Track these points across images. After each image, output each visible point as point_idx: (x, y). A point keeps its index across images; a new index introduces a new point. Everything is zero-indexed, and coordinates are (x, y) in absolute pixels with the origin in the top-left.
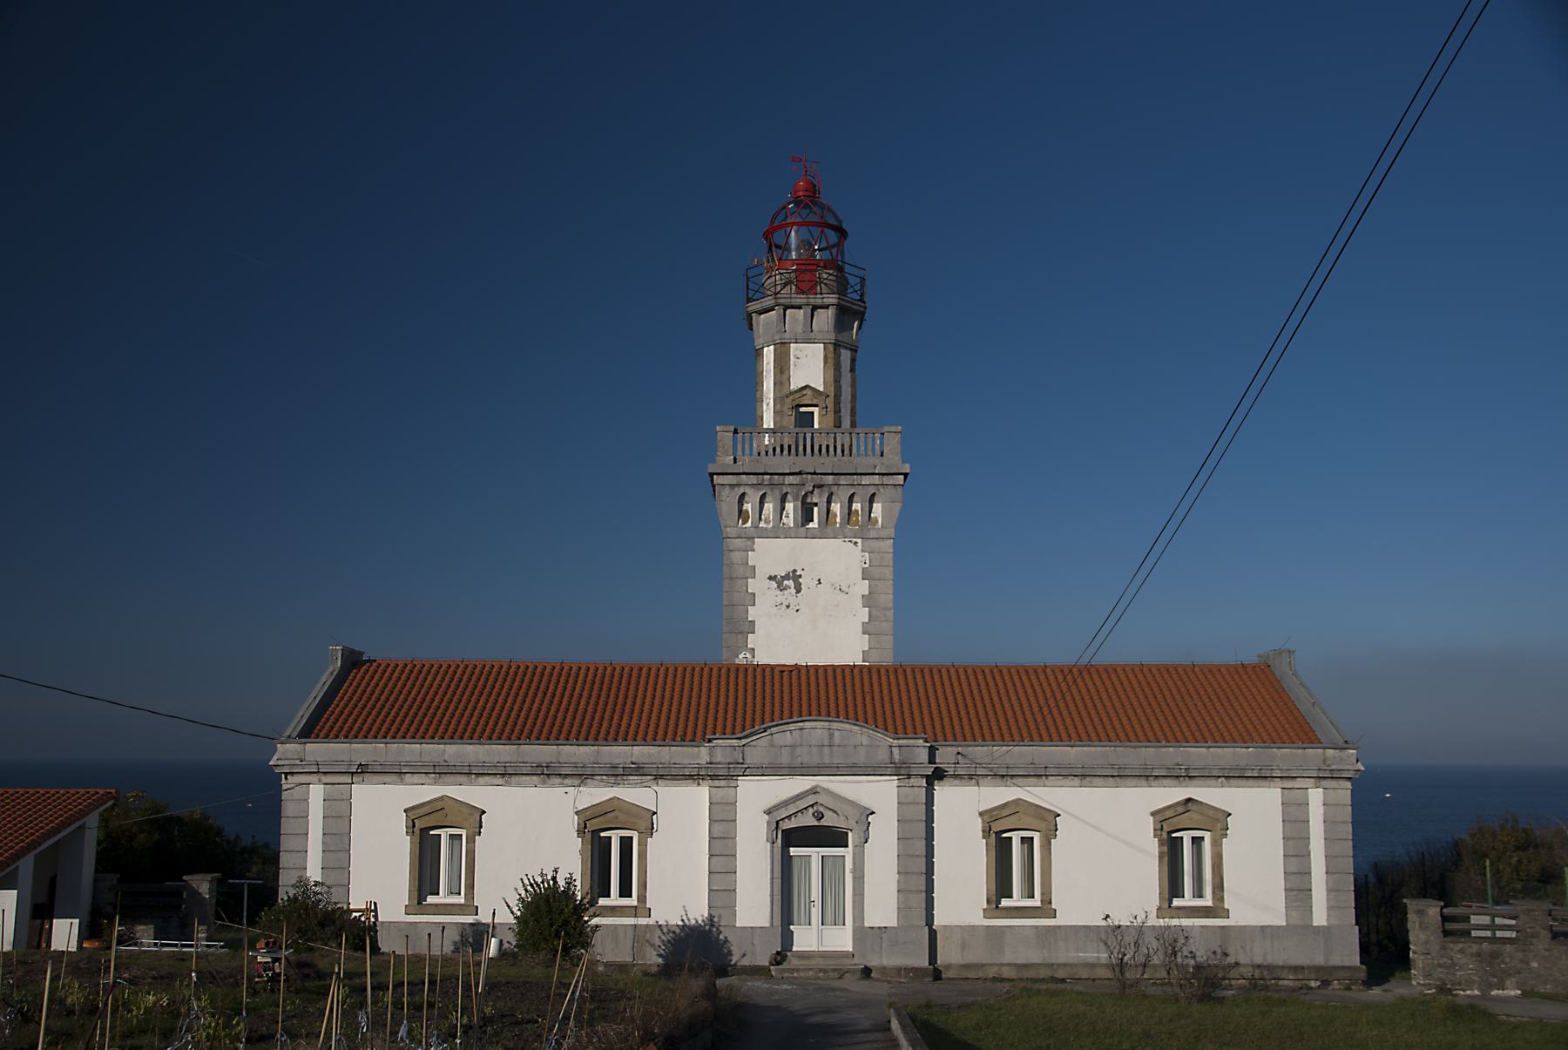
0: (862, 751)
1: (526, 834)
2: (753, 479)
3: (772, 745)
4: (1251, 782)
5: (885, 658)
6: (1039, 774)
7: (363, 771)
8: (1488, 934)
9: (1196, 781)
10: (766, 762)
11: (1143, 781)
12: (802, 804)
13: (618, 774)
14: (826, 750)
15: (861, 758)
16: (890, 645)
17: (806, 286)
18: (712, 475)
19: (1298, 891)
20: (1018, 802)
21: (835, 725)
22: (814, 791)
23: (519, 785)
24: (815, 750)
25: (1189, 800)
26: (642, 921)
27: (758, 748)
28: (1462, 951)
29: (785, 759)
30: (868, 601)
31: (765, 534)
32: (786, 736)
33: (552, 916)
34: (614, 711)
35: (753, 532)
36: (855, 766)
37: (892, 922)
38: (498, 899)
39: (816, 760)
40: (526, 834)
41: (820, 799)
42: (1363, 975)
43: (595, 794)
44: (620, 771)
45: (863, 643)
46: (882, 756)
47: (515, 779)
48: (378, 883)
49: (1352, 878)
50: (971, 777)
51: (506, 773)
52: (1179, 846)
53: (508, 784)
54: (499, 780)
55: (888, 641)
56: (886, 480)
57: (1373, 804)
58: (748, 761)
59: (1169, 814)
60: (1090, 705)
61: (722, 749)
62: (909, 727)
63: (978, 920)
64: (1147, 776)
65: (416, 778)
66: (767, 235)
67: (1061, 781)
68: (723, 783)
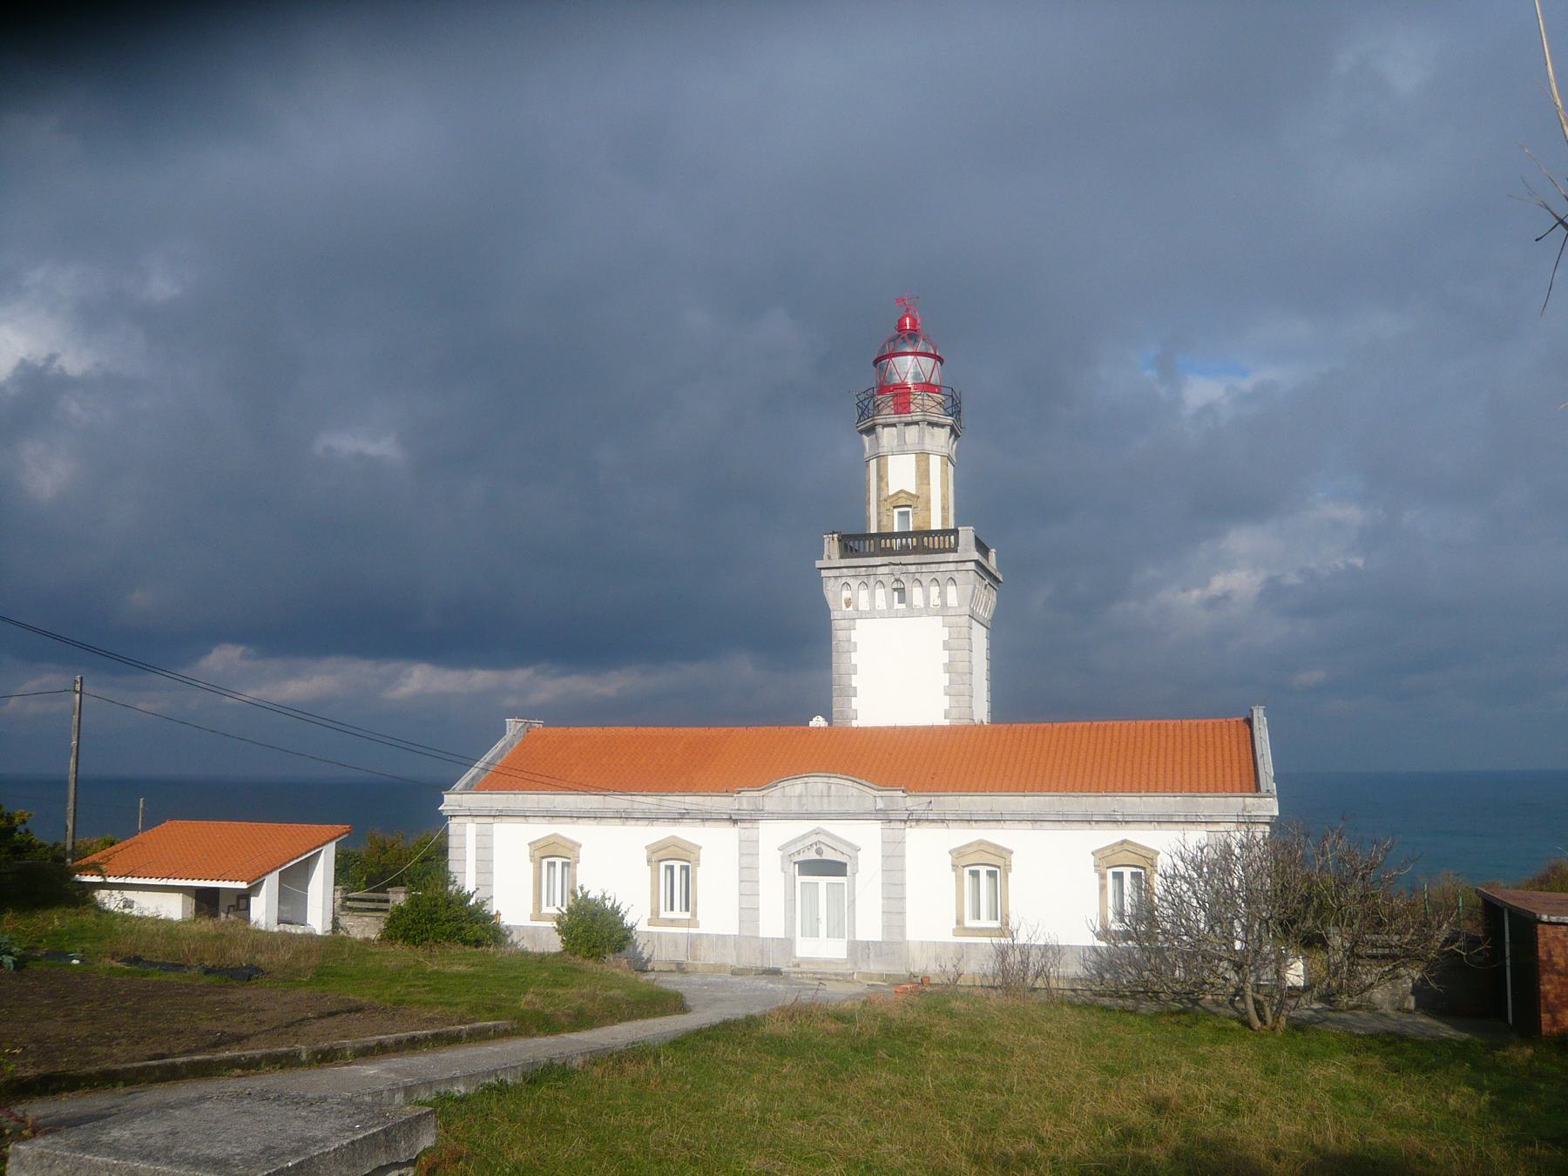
6: (998, 819)
7: (500, 815)
11: (1086, 825)
12: (807, 842)
14: (825, 800)
15: (852, 808)
19: (485, 848)
20: (981, 842)
21: (1249, 800)
22: (817, 832)
26: (693, 931)
27: (773, 798)
32: (795, 788)
39: (817, 808)
41: (822, 838)
45: (945, 702)
46: (868, 805)
50: (943, 821)
52: (986, 868)
56: (961, 566)
59: (1108, 852)
61: (745, 801)
67: (1017, 825)
68: (748, 825)
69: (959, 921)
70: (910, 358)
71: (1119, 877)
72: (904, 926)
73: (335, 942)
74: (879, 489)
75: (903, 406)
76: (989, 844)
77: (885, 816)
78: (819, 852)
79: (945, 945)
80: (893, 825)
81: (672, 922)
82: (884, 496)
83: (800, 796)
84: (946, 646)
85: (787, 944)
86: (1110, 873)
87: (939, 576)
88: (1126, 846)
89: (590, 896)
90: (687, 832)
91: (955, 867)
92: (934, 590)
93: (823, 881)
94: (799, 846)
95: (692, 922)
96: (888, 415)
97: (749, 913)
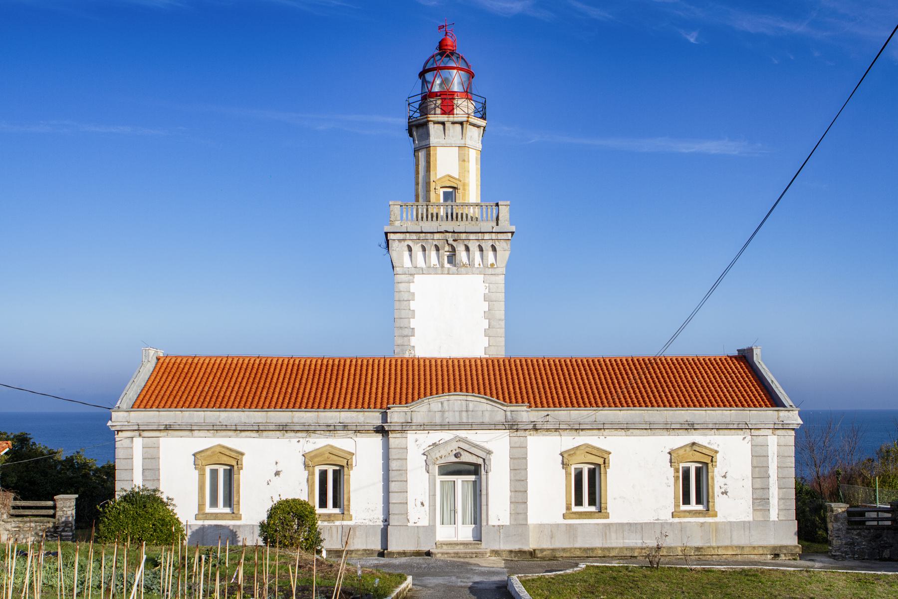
1: (274, 466)
2: (414, 237)
3: (429, 411)
4: (733, 431)
5: (499, 352)
6: (600, 428)
8: (875, 523)
9: (698, 431)
10: (426, 421)
11: (665, 432)
13: (331, 429)
14: (464, 414)
16: (503, 344)
17: (447, 109)
18: (386, 234)
19: (761, 501)
21: (470, 398)
23: (267, 437)
25: (694, 444)
28: (859, 534)
30: (488, 315)
31: (422, 272)
33: (289, 523)
34: (477, 375)
35: (413, 271)
36: (482, 424)
37: (508, 524)
38: (253, 511)
39: (457, 420)
40: (274, 466)
42: (798, 550)
43: (319, 442)
44: (332, 428)
45: (485, 342)
47: (265, 433)
48: (185, 497)
49: (794, 491)
50: (556, 430)
51: (259, 430)
53: (260, 437)
54: (254, 434)
55: (502, 341)
56: (500, 236)
57: (807, 443)
58: (414, 421)
60: (516, 381)
62: (458, 386)
64: (668, 428)
65: (202, 433)
66: (422, 75)
68: (399, 435)
69: (568, 508)
70: (455, 71)
71: (214, 473)
72: (526, 514)
75: (448, 110)
76: (594, 448)
77: (512, 426)
78: (456, 456)
80: (519, 433)
81: (216, 516)
85: (431, 529)
86: (208, 470)
88: (695, 448)
89: (158, 494)
90: (342, 443)
91: (306, 466)
95: (235, 515)
96: (437, 116)
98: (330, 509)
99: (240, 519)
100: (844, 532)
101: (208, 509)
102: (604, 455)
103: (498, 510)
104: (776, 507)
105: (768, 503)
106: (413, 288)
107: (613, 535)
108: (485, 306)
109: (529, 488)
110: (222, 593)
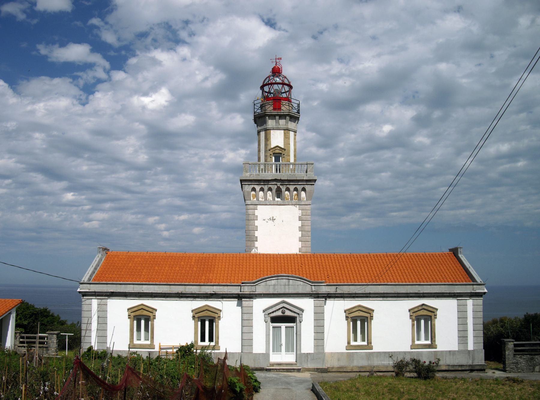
0: (301, 287)
5: (308, 250)
14: (287, 287)
19: (463, 338)
20: (360, 306)
24: (283, 287)
29: (271, 291)
30: (301, 229)
37: (312, 352)
39: (282, 292)
45: (299, 245)
52: (360, 320)
63: (409, 349)
69: (349, 343)
73: (15, 353)
74: (266, 145)
77: (316, 296)
78: (283, 313)
79: (342, 353)
82: (269, 148)
83: (274, 285)
84: (300, 219)
85: (266, 356)
87: (298, 187)
88: (424, 307)
92: (261, 193)
93: (283, 326)
94: (274, 309)
97: (247, 340)
98: (207, 343)
99: (154, 349)
100: (512, 356)
101: (353, 343)
102: (370, 311)
103: (307, 345)
104: (96, 322)
105: (467, 340)
106: (257, 213)
107: (375, 359)
108: (299, 224)
109: (327, 330)
110: (120, 398)
